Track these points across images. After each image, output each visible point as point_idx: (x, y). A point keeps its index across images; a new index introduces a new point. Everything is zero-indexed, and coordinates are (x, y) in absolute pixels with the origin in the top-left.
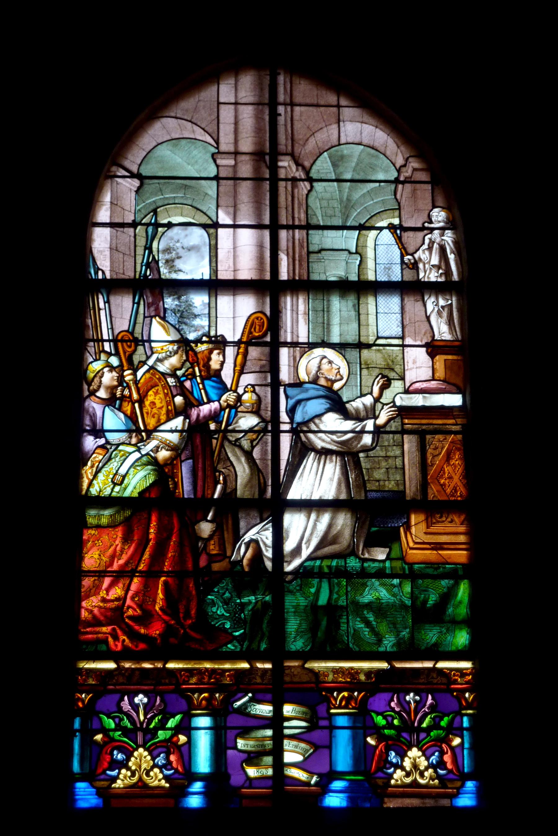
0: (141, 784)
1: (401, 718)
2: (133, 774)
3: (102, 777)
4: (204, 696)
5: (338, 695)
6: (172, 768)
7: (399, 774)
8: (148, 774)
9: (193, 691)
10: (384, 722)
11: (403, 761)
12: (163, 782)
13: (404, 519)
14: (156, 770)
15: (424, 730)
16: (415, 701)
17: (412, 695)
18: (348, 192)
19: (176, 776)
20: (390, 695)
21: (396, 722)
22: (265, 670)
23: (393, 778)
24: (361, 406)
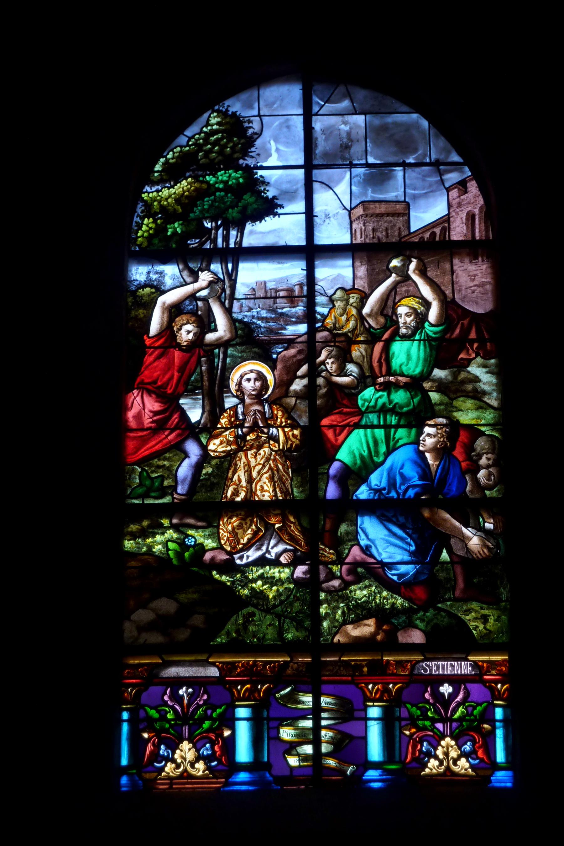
0: (185, 775)
1: (175, 711)
2: (441, 763)
3: (150, 768)
4: (247, 688)
5: (242, 688)
6: (478, 758)
7: (169, 767)
8: (455, 764)
9: (237, 683)
10: (156, 715)
11: (174, 753)
12: (470, 770)
13: (132, 528)
14: (463, 760)
15: (456, 720)
16: (188, 694)
17: (184, 688)
18: (485, 234)
19: (483, 765)
20: (163, 688)
21: (170, 716)
22: (307, 663)
23: (428, 767)
24: (470, 414)
